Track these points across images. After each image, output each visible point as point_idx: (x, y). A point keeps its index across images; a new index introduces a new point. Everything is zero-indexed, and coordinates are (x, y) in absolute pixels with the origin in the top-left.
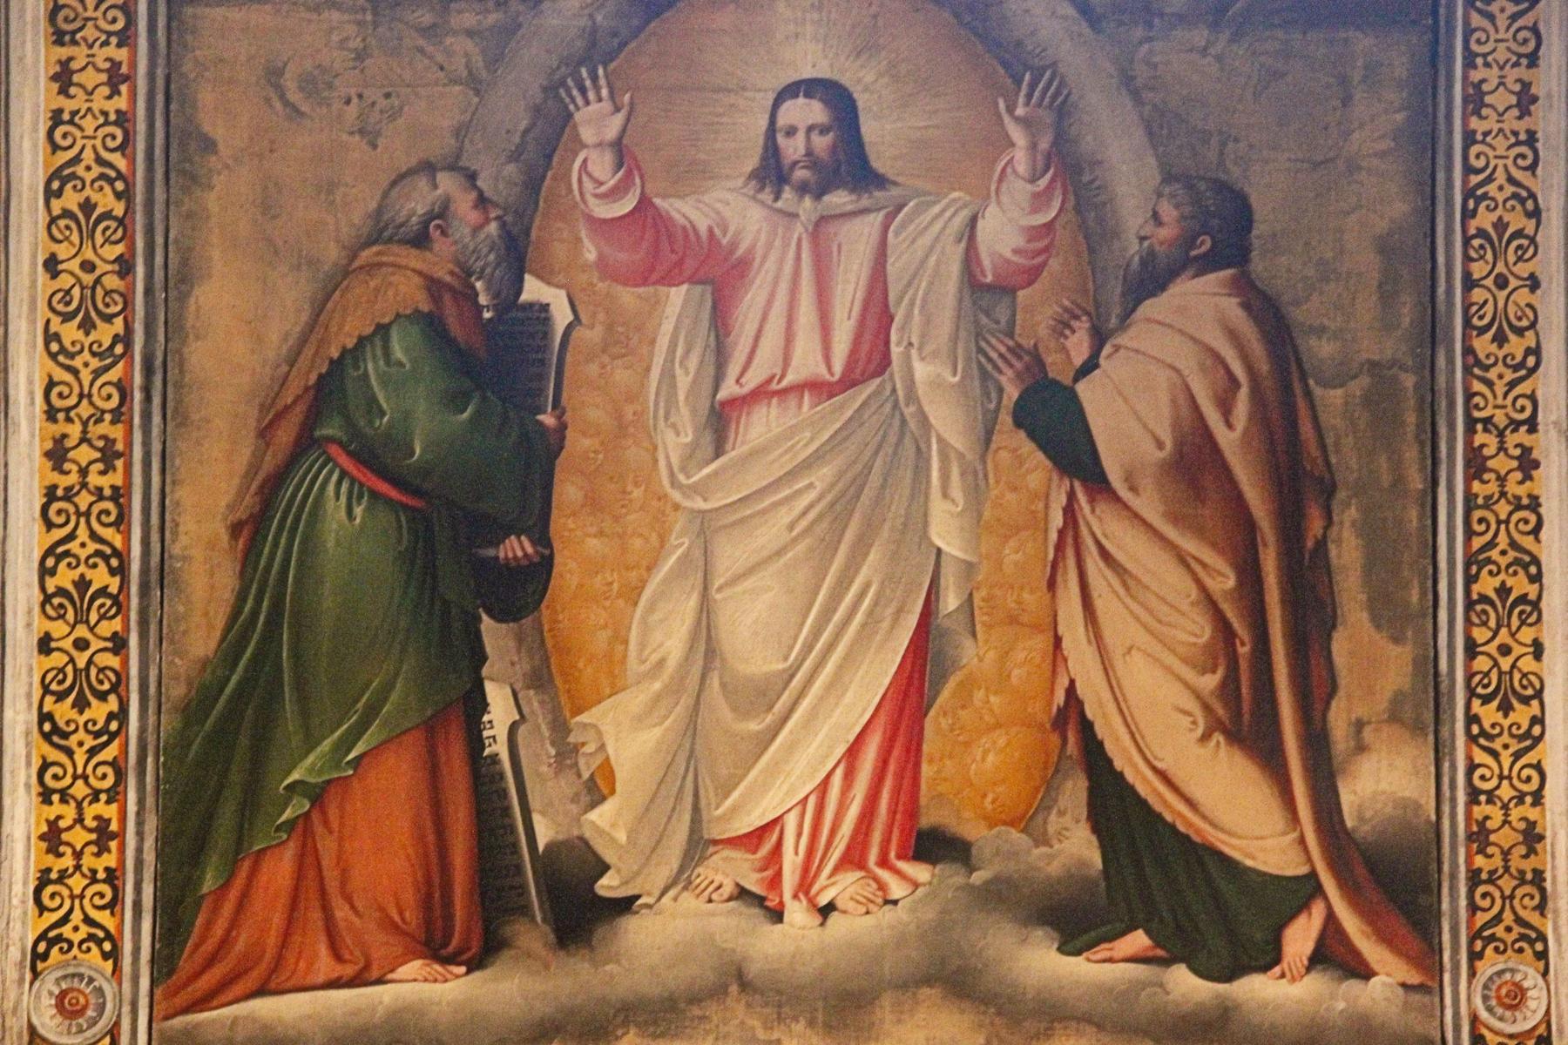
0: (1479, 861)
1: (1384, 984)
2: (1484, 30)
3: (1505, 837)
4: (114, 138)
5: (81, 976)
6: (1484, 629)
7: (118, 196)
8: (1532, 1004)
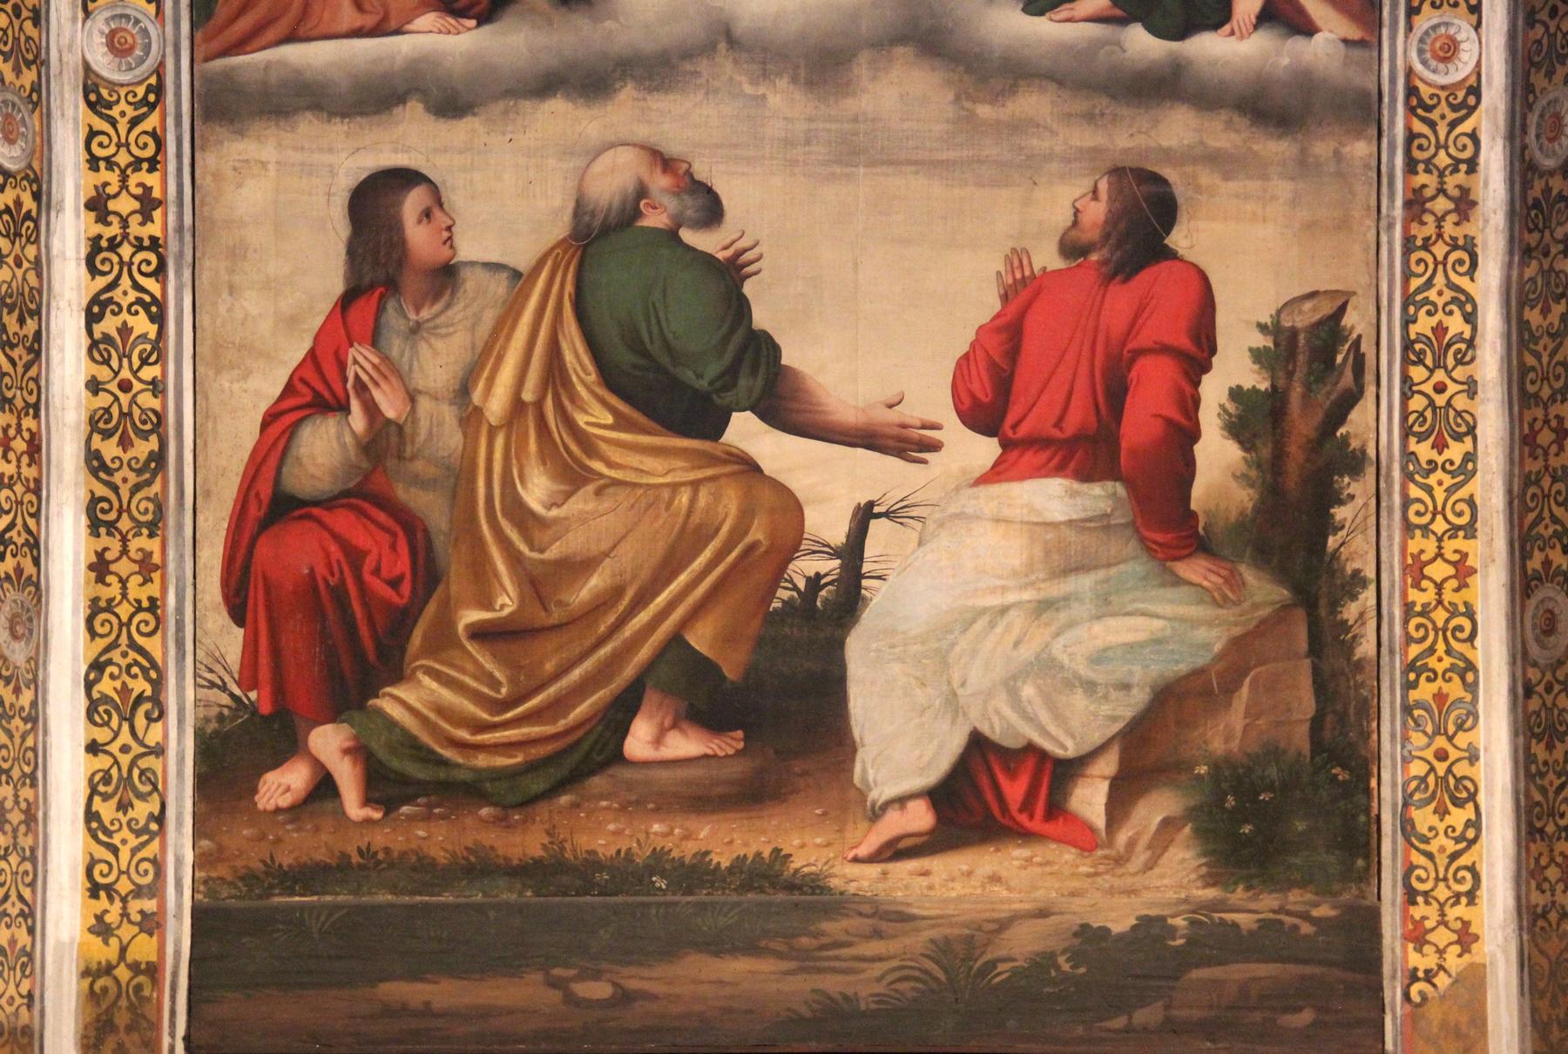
0: (1413, 595)
1: (1326, 39)
2: (1426, 137)
3: (1439, 570)
4: (149, 263)
5: (127, 17)
6: (1421, 368)
7: (152, 319)
8: (1464, 56)
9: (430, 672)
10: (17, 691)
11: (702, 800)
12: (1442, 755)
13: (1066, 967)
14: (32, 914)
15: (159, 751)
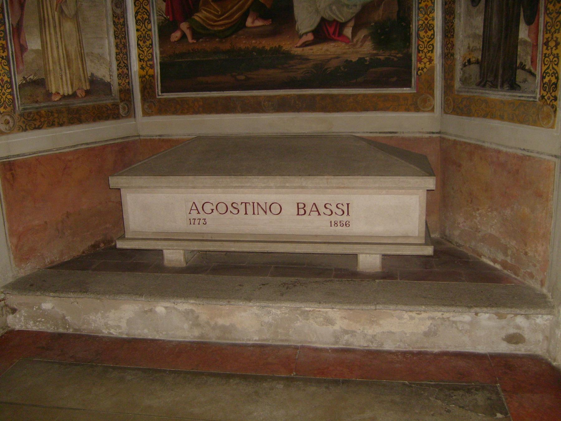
9: (205, 10)
10: (119, 19)
11: (262, 34)
12: (426, 19)
13: (343, 69)
14: (127, 66)
15: (150, 30)
